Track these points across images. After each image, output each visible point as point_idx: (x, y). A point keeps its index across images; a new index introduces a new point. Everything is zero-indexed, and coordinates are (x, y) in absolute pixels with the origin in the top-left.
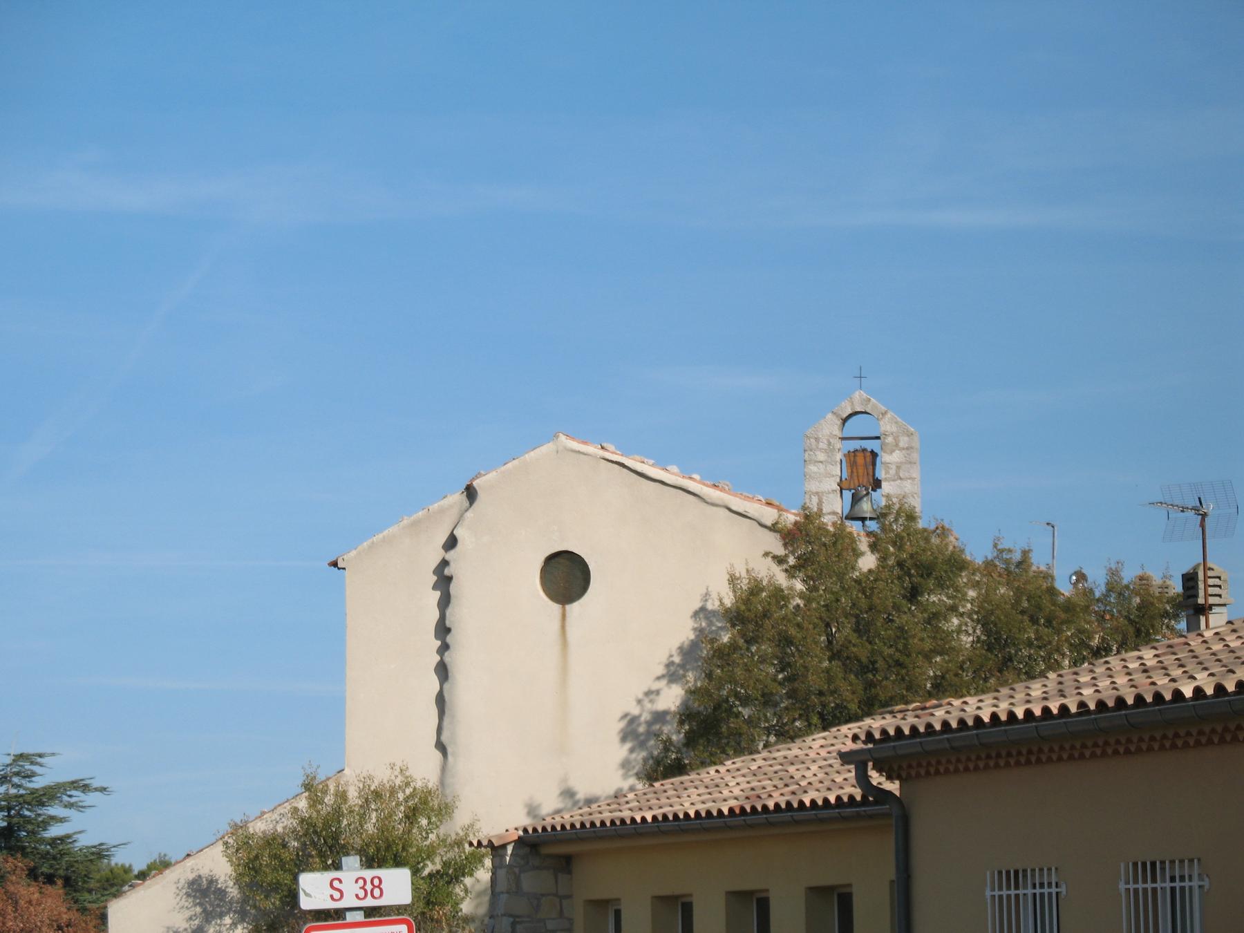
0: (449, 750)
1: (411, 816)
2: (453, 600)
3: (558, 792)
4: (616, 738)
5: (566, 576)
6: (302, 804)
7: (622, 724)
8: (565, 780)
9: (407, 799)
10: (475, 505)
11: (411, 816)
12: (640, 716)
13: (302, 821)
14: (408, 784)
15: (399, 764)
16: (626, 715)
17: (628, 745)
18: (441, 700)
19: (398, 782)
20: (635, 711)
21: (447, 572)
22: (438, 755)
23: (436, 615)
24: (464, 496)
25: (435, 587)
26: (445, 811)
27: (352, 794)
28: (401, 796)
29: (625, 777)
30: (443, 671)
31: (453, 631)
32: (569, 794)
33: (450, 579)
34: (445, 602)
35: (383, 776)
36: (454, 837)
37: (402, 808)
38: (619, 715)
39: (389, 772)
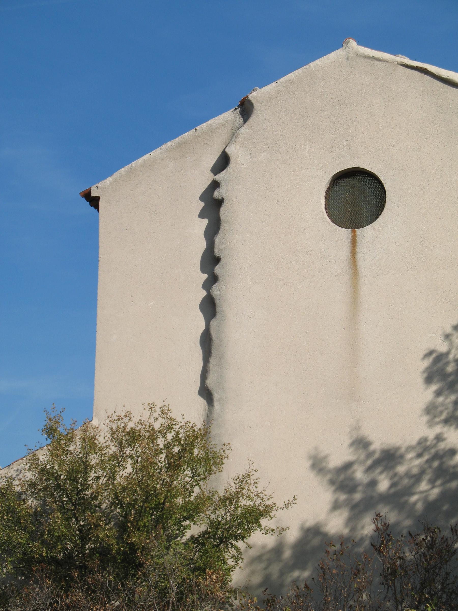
0: (216, 396)
1: (174, 465)
2: (223, 226)
3: (348, 441)
4: (419, 380)
5: (357, 196)
6: (43, 456)
7: (427, 363)
8: (357, 428)
9: (168, 446)
10: (251, 120)
11: (174, 465)
12: (448, 353)
13: (43, 471)
14: (170, 428)
15: (159, 404)
16: (431, 353)
17: (434, 387)
18: (207, 341)
19: (157, 426)
20: (443, 348)
21: (217, 194)
22: (202, 402)
23: (202, 245)
24: (237, 114)
25: (202, 215)
26: (211, 462)
27: (102, 439)
28: (161, 442)
29: (431, 424)
30: (210, 307)
31: (222, 262)
32: (361, 443)
33: (219, 203)
34: (214, 229)
35: (140, 416)
36: (222, 493)
37: (163, 456)
38: (424, 352)
39: (147, 414)
